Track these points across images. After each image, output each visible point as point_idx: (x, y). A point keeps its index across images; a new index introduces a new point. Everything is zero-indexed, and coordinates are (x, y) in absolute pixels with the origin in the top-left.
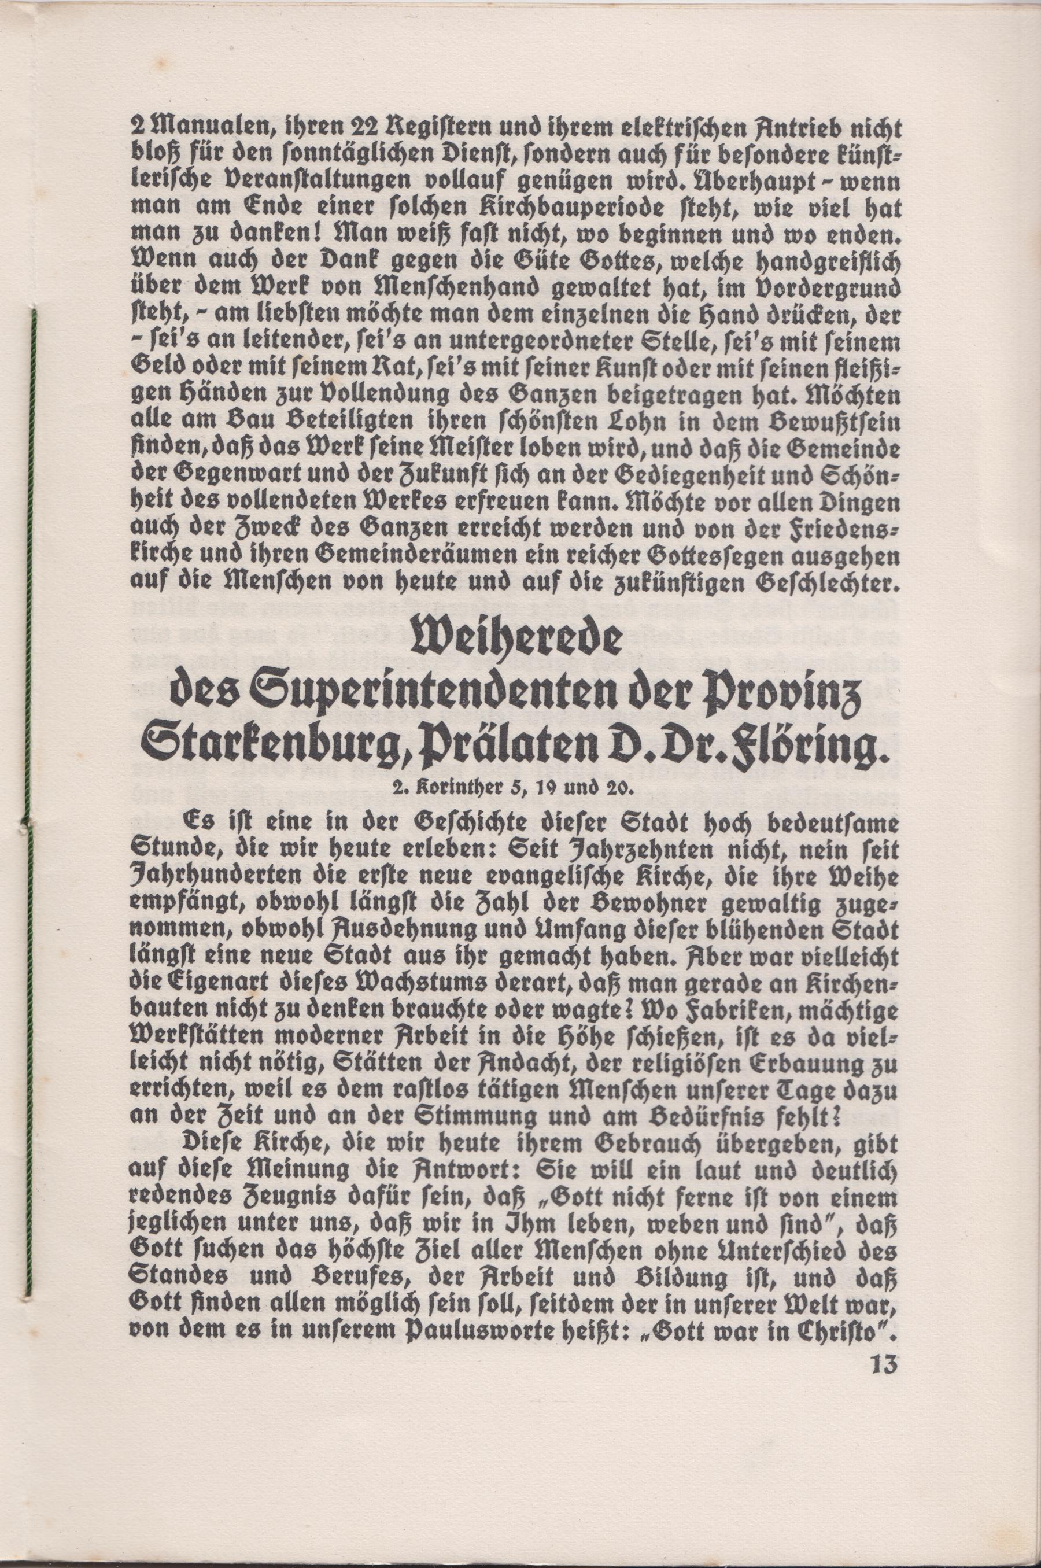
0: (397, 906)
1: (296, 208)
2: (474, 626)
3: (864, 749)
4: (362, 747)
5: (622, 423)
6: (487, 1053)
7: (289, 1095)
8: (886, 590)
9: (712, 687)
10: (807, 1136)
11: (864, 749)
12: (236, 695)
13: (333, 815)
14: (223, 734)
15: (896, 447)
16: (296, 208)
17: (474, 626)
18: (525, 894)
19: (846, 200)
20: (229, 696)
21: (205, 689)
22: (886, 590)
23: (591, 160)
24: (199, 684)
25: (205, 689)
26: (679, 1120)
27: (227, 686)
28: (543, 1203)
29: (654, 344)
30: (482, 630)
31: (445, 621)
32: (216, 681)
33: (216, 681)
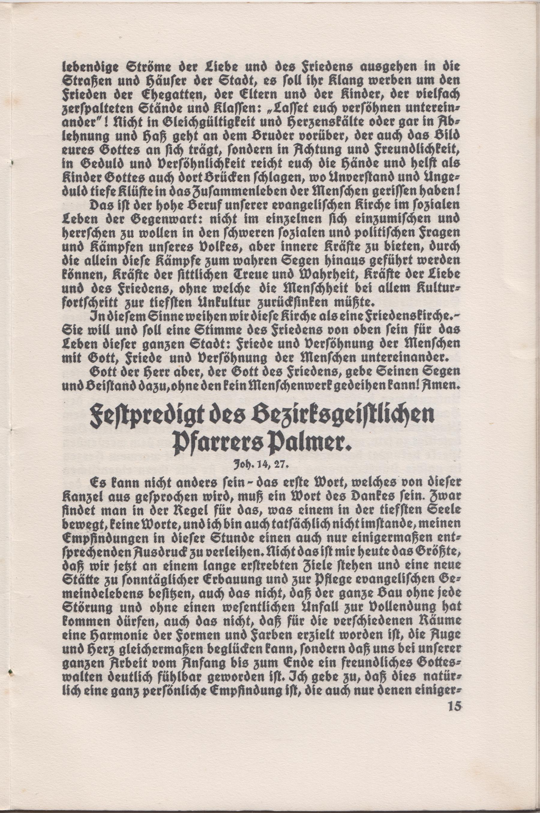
0: (226, 652)
1: (159, 359)
2: (355, 409)
3: (189, 416)
4: (302, 417)
5: (69, 345)
6: (435, 629)
7: (160, 333)
8: (339, 448)
9: (273, 440)
10: (342, 353)
11: (189, 416)
12: (244, 417)
13: (428, 63)
14: (210, 437)
15: (459, 591)
16: (159, 359)
17: (355, 409)
18: (458, 187)
19: (206, 506)
20: (325, 418)
21: (228, 414)
22: (339, 448)
23: (161, 652)
24: (225, 412)
25: (228, 414)
26: (377, 622)
27: (324, 413)
28: (269, 111)
29: (69, 331)
30: (359, 411)
31: (324, 478)
32: (233, 410)
33: (233, 410)
